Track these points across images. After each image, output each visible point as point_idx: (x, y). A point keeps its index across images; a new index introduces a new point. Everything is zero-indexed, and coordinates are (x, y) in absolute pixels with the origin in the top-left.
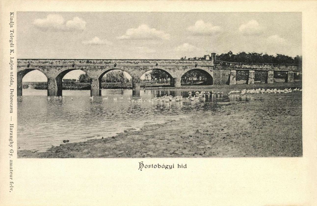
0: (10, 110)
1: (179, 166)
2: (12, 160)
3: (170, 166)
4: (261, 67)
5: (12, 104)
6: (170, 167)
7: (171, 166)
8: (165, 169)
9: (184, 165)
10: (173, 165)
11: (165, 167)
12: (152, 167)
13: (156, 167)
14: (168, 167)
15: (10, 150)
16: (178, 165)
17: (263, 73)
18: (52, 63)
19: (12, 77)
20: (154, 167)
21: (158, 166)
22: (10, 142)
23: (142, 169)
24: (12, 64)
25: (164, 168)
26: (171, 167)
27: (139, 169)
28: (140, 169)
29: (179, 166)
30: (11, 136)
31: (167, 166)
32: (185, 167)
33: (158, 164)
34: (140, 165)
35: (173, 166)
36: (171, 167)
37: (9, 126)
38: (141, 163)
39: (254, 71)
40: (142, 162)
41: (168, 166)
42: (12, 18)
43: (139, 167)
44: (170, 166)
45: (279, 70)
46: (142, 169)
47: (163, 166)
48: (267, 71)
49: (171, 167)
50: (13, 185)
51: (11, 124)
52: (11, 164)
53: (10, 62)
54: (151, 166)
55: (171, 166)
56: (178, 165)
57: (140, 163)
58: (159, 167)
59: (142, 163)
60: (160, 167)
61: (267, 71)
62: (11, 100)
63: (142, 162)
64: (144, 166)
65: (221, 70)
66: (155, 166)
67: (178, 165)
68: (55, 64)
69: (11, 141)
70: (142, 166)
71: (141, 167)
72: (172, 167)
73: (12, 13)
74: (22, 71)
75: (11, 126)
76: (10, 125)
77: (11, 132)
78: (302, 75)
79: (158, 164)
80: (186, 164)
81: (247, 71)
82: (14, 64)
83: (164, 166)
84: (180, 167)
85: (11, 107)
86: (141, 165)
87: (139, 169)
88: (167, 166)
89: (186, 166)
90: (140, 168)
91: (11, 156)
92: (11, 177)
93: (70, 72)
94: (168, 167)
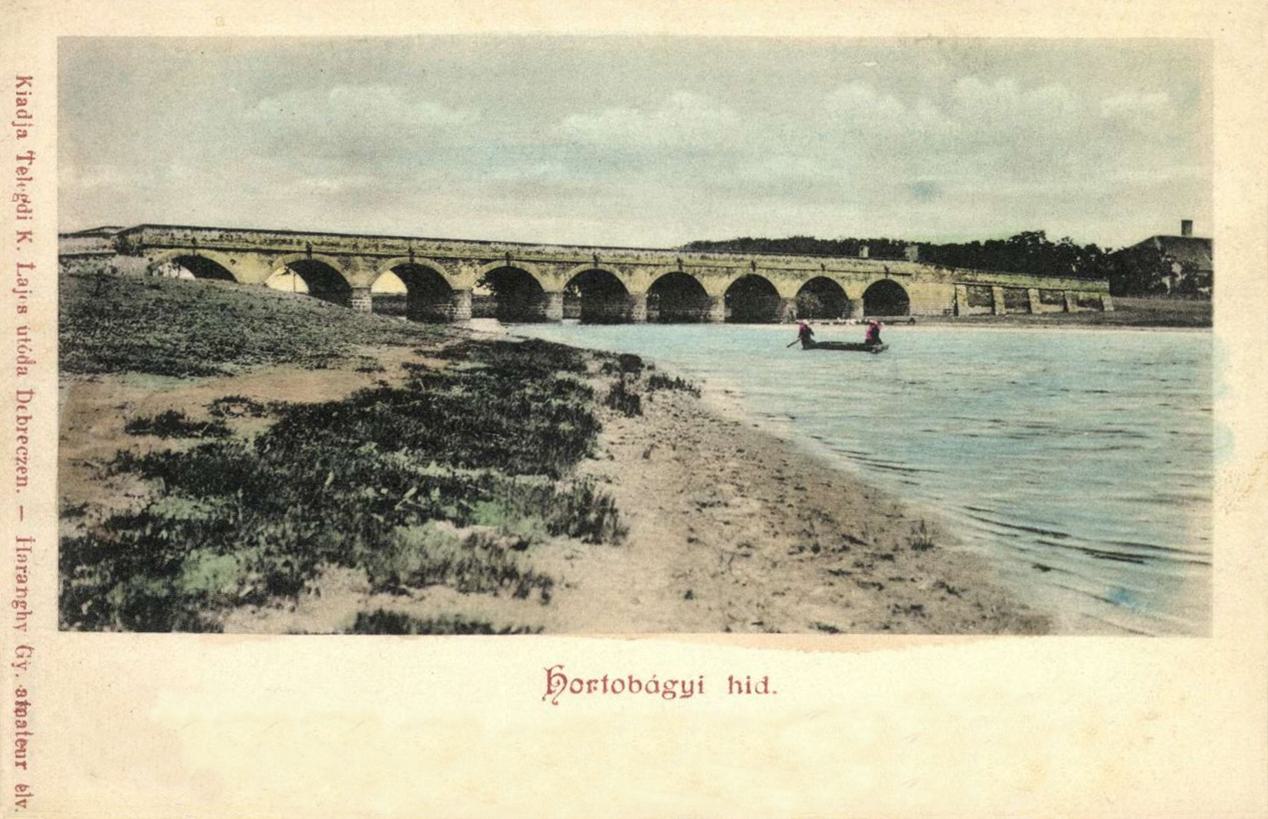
1: (735, 687)
2: (29, 278)
3: (683, 683)
4: (1014, 281)
5: (23, 451)
6: (684, 691)
7: (692, 683)
8: (663, 696)
9: (756, 680)
10: (699, 680)
11: (662, 689)
13: (614, 683)
14: (678, 689)
15: (20, 645)
16: (731, 679)
17: (1018, 292)
18: (638, 258)
19: (23, 346)
20: (614, 691)
21: (631, 683)
22: (18, 613)
23: (557, 699)
24: (26, 292)
25: (654, 694)
26: (688, 687)
27: (544, 699)
28: (549, 698)
29: (735, 687)
30: (22, 586)
31: (669, 685)
32: (761, 688)
33: (630, 678)
34: (549, 679)
35: (701, 684)
36: (692, 691)
37: (14, 544)
38: (553, 673)
39: (1001, 289)
40: (561, 667)
41: (674, 683)
42: (22, 97)
43: (546, 689)
44: (683, 683)
45: (1047, 287)
46: (557, 699)
47: (652, 687)
48: (1027, 289)
49: (688, 687)
51: (22, 538)
52: (22, 707)
54: (600, 685)
55: (692, 683)
56: (731, 679)
57: (549, 671)
58: (635, 686)
59: (556, 670)
60: (640, 688)
61: (1027, 289)
62: (21, 433)
63: (561, 667)
64: (568, 685)
66: (618, 686)
67: (728, 682)
68: (643, 260)
69: (20, 609)
70: (559, 683)
71: (552, 688)
72: (696, 688)
73: (25, 233)
74: (821, 650)
75: (21, 545)
76: (19, 540)
77: (21, 572)
79: (630, 678)
80: (766, 678)
81: (989, 287)
82: (30, 93)
83: (657, 683)
84: (740, 691)
85: (21, 464)
86: (555, 681)
87: (544, 699)
88: (669, 685)
89: (766, 684)
90: (550, 692)
91: (20, 671)
92: (21, 760)
94: (678, 689)
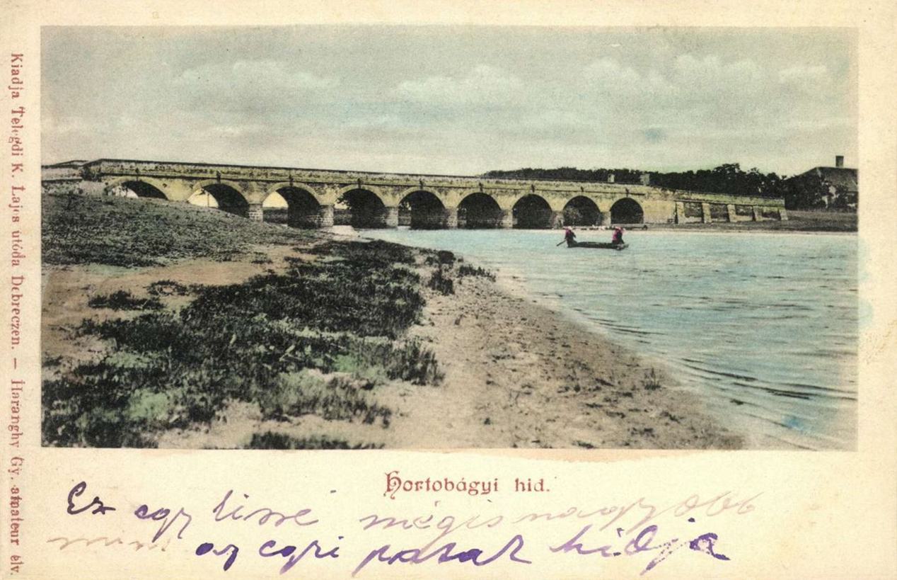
0: (12, 125)
1: (520, 487)
3: (483, 484)
5: (16, 319)
6: (484, 490)
7: (489, 483)
8: (469, 493)
9: (535, 482)
10: (494, 482)
11: (468, 488)
12: (428, 489)
13: (434, 484)
14: (479, 488)
15: (14, 456)
16: (517, 481)
17: (720, 207)
20: (434, 489)
21: (446, 483)
22: (13, 434)
23: (394, 495)
24: (18, 207)
25: (463, 492)
26: (486, 486)
27: (385, 495)
28: (389, 494)
29: (520, 487)
30: (15, 415)
31: (474, 485)
32: (538, 487)
33: (446, 480)
34: (389, 481)
35: (496, 484)
36: (489, 489)
37: (10, 385)
38: (391, 476)
39: (708, 204)
40: (397, 472)
41: (477, 484)
42: (16, 69)
44: (483, 484)
45: (741, 203)
46: (394, 495)
47: (461, 486)
48: (727, 205)
49: (486, 486)
50: (11, 212)
51: (16, 381)
52: (15, 501)
53: (11, 202)
54: (425, 485)
55: (489, 483)
56: (517, 481)
57: (389, 476)
58: (449, 486)
59: (394, 475)
60: (453, 487)
61: (727, 205)
62: (15, 307)
63: (397, 472)
64: (402, 485)
65: (658, 201)
66: (437, 486)
67: (515, 483)
69: (14, 432)
70: (395, 484)
71: (391, 488)
72: (493, 487)
73: (18, 165)
75: (15, 386)
76: (13, 383)
77: (15, 405)
78: (501, 230)
79: (446, 480)
80: (542, 480)
81: (699, 204)
83: (464, 484)
84: (524, 489)
85: (15, 329)
87: (385, 495)
88: (474, 485)
89: (542, 484)
90: (389, 490)
91: (14, 475)
92: (15, 538)
93: (553, 168)
94: (479, 488)
